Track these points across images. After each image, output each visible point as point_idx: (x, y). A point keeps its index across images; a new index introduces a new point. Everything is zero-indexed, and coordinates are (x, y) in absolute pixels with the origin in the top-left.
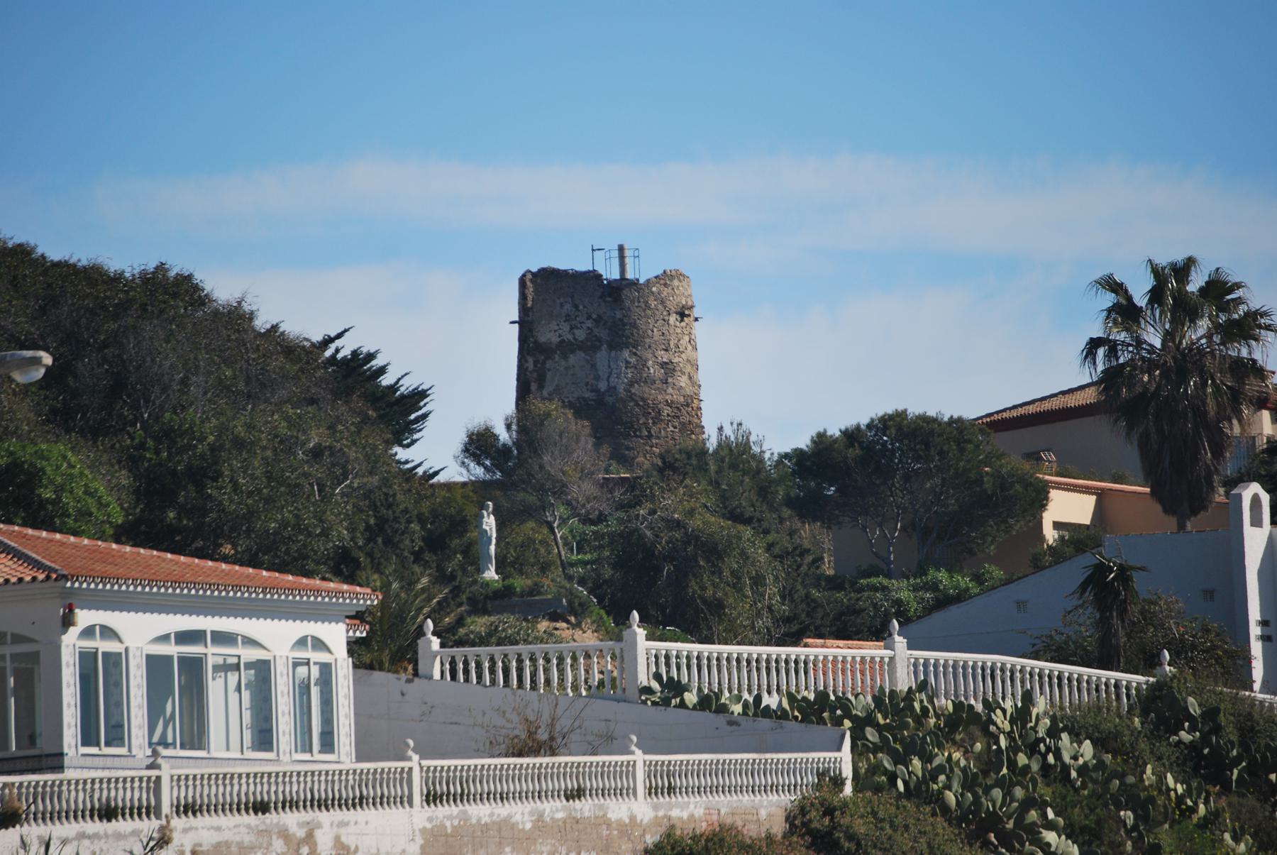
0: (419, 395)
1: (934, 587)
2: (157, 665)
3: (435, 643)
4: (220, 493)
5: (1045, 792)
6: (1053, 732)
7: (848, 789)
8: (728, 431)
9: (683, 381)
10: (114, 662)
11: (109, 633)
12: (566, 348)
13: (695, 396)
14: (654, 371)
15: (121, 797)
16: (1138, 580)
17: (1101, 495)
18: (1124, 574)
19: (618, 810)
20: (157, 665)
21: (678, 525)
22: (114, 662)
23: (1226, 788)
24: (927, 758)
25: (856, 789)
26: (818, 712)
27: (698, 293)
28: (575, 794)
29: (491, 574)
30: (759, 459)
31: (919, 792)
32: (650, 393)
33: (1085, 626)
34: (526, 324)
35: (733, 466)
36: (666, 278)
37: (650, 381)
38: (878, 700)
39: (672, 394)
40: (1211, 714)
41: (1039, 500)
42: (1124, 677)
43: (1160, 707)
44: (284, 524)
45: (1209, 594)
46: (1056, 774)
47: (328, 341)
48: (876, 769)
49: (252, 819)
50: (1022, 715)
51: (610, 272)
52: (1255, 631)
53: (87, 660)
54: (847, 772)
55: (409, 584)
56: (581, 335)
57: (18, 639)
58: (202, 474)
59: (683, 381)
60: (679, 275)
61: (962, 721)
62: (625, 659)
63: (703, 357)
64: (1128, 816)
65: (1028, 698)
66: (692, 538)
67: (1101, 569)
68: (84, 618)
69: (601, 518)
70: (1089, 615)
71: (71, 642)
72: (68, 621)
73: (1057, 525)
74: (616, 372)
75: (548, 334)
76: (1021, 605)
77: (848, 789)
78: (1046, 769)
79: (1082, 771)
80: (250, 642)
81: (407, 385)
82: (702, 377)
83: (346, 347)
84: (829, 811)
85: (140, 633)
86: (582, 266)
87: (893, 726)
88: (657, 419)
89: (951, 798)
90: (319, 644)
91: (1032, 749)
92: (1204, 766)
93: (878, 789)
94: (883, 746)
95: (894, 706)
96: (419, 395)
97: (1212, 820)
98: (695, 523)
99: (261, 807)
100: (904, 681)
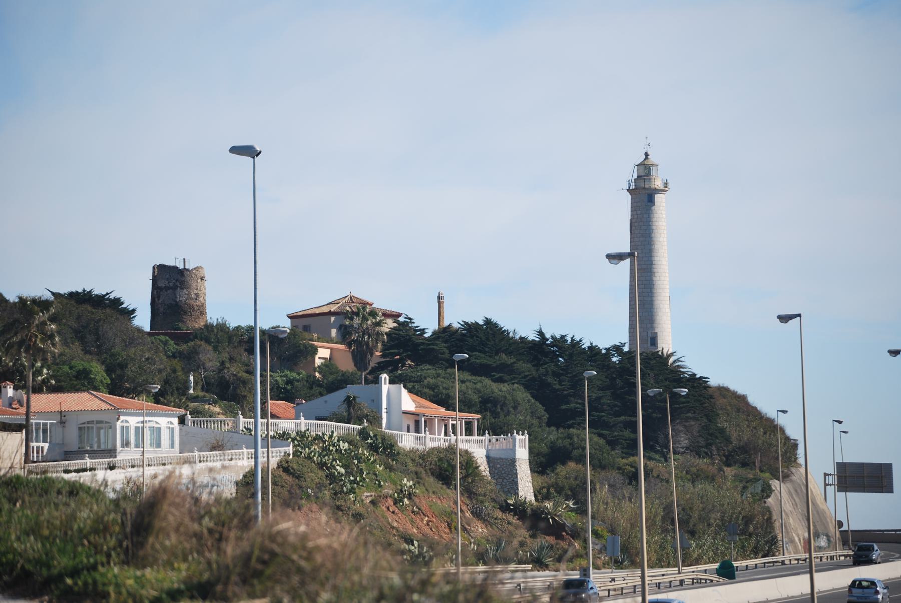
0: (134, 311)
1: (286, 376)
2: (137, 428)
3: (190, 417)
4: (128, 372)
5: (336, 456)
6: (338, 441)
7: (291, 457)
8: (220, 320)
9: (201, 299)
10: (127, 428)
11: (127, 422)
12: (167, 288)
13: (204, 304)
14: (193, 296)
15: (135, 463)
16: (358, 400)
17: (332, 349)
18: (354, 398)
19: (240, 463)
20: (137, 428)
21: (235, 375)
22: (127, 428)
23: (378, 453)
24: (309, 449)
25: (294, 456)
26: (283, 437)
27: (207, 273)
28: (231, 460)
29: (191, 391)
30: (228, 328)
31: (309, 458)
32: (192, 302)
33: (343, 410)
34: (155, 281)
35: (221, 331)
36: (197, 269)
37: (192, 299)
38: (297, 433)
39: (198, 303)
40: (375, 436)
41: (315, 350)
42: (355, 426)
43: (363, 434)
44: (144, 381)
45: (373, 401)
46: (339, 451)
47: (107, 294)
48: (297, 451)
49: (162, 467)
50: (331, 437)
51: (181, 267)
52: (384, 411)
53: (122, 427)
54: (291, 452)
55: (180, 400)
56: (171, 284)
57: (106, 422)
58: (123, 366)
59: (201, 299)
60: (201, 268)
61: (318, 438)
62: (236, 424)
63: (207, 292)
64: (356, 462)
65: (332, 432)
66: (239, 379)
67: (349, 397)
68: (122, 418)
69: (410, 541)
70: (345, 406)
71: (119, 424)
72: (118, 419)
73: (320, 358)
74: (182, 296)
75: (162, 284)
76: (326, 402)
77: (291, 457)
78: (337, 450)
79: (345, 450)
80: (157, 423)
81: (131, 308)
82: (207, 298)
83: (112, 296)
84: (287, 462)
85: (133, 421)
86: (172, 264)
87: (301, 438)
88: (194, 310)
89: (315, 458)
90: (171, 423)
91: (334, 445)
92: (373, 448)
93: (298, 456)
94: (299, 445)
95: (302, 435)
96: (134, 311)
97: (375, 461)
98: (240, 375)
99: (164, 464)
100: (303, 429)
